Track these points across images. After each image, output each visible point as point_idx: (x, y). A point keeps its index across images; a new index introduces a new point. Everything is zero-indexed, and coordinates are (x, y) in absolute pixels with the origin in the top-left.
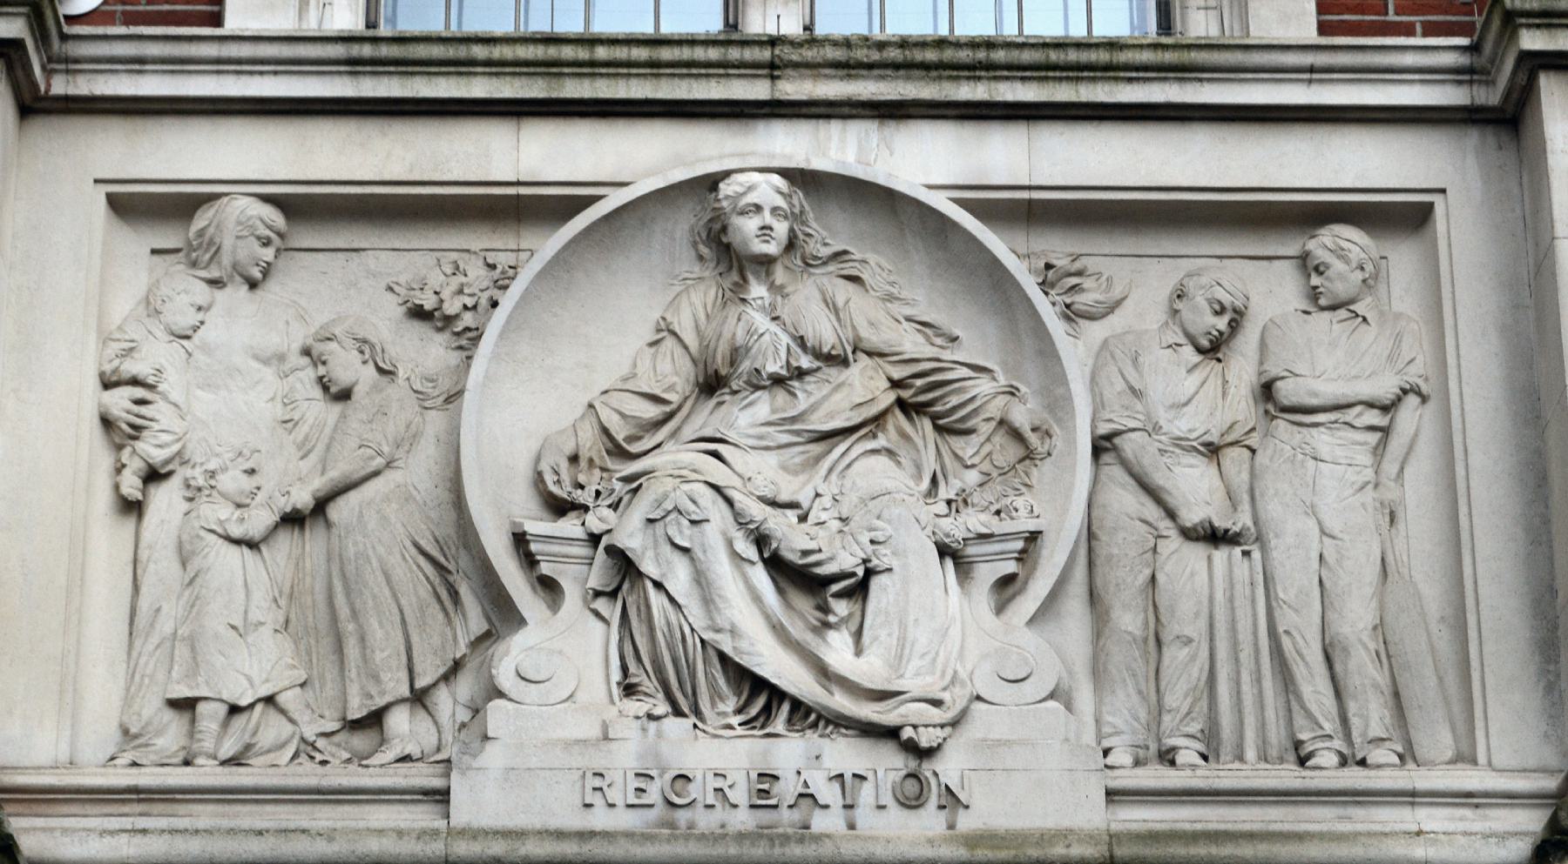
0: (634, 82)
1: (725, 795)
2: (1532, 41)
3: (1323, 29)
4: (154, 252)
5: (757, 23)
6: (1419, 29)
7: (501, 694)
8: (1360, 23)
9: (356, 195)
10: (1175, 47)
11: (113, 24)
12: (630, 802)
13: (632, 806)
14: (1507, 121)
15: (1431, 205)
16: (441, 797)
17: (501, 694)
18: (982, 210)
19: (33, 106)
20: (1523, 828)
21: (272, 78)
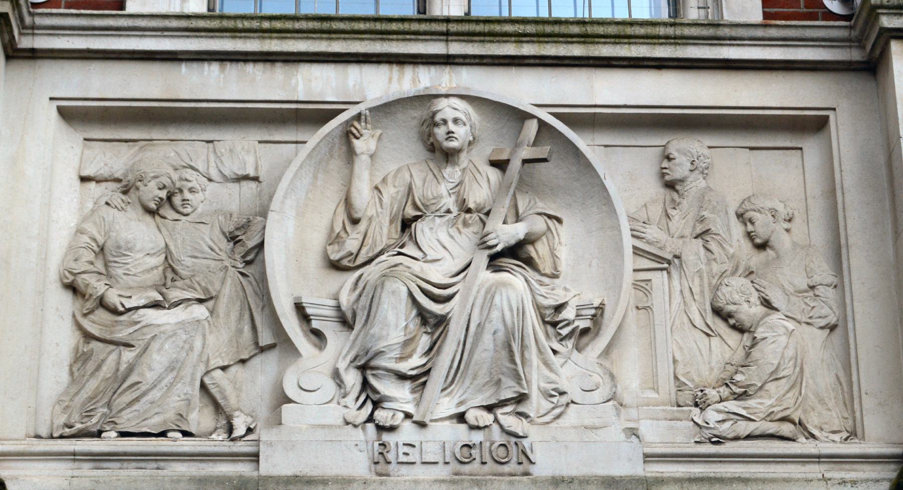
0: (657, 47)
1: (384, 457)
2: (888, 22)
3: (766, 16)
4: (85, 139)
5: (438, 10)
6: (820, 15)
7: (290, 401)
8: (776, 13)
9: (206, 108)
10: (426, 20)
11: (817, 20)
12: (400, 460)
13: (402, 463)
14: (872, 67)
15: (827, 117)
16: (255, 457)
17: (290, 401)
18: (571, 120)
19: (14, 54)
20: (886, 477)
21: (138, 39)
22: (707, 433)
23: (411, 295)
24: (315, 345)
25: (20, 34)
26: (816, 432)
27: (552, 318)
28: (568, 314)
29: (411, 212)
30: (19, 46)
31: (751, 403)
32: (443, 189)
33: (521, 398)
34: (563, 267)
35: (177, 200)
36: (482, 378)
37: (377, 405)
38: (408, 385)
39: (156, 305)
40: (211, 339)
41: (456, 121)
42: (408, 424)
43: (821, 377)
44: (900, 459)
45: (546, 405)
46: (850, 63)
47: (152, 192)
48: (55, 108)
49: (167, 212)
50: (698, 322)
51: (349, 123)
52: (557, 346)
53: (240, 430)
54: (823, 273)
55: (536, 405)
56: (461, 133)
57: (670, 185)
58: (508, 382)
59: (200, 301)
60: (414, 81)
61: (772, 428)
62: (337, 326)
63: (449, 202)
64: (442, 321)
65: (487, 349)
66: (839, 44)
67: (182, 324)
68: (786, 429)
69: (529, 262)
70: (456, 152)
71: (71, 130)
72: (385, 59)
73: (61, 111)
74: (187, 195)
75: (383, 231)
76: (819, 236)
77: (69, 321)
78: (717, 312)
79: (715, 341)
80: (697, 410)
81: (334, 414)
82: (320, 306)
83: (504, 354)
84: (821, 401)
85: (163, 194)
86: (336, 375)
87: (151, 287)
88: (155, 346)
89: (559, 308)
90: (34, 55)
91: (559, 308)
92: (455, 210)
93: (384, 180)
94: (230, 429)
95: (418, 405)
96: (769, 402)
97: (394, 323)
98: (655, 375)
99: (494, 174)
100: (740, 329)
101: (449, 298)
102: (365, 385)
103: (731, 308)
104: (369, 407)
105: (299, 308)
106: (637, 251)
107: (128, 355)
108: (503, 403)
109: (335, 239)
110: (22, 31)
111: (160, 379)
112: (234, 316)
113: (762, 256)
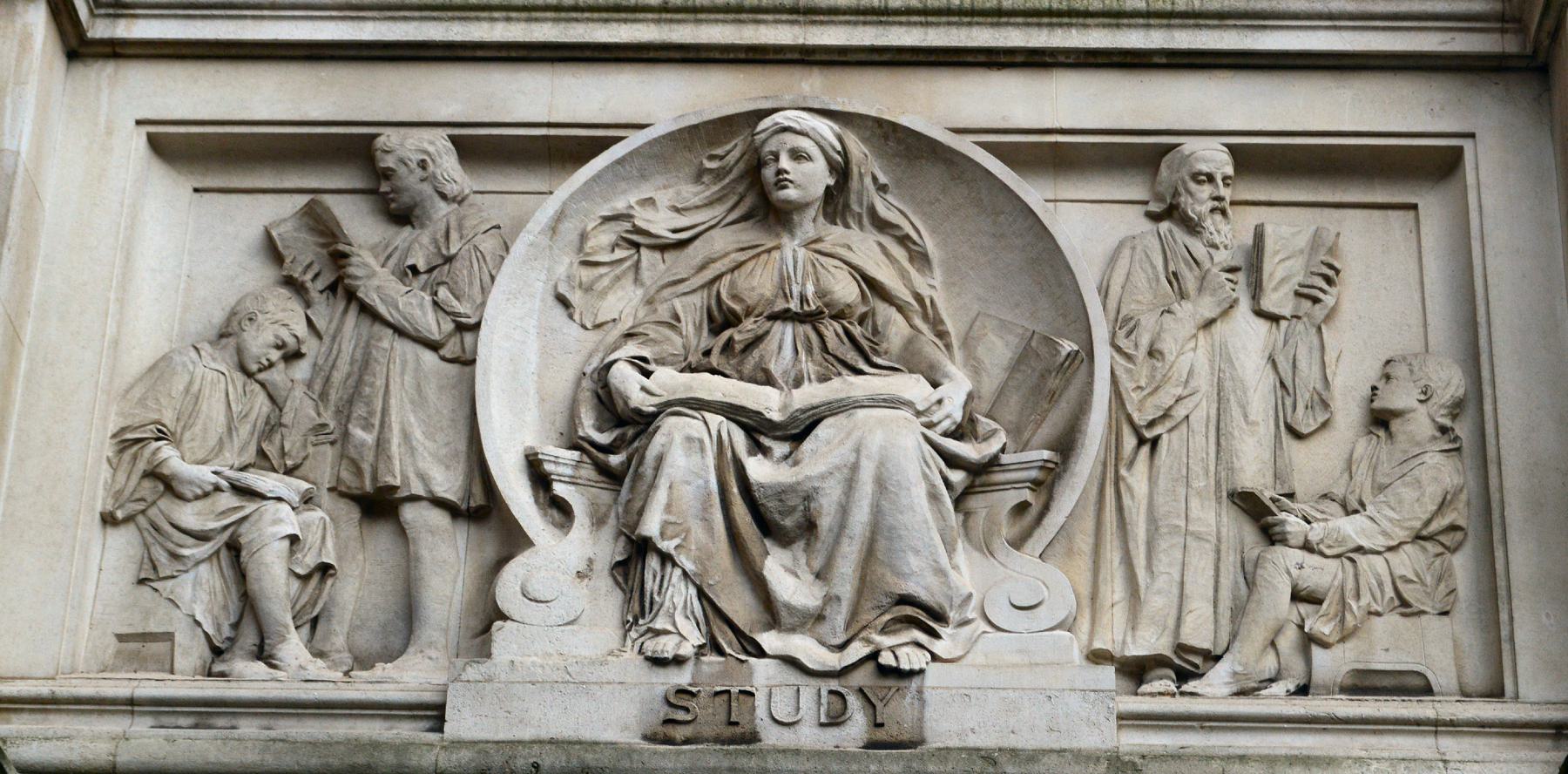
4: (196, 190)
7: (504, 617)
15: (1460, 150)
17: (504, 617)
24: (555, 524)
25: (92, 14)
30: (90, 35)
44: (1560, 731)
46: (1502, 57)
48: (144, 138)
66: (1478, 25)
71: (173, 174)
72: (108, 50)
87: (655, 416)
90: (117, 51)
110: (96, 12)
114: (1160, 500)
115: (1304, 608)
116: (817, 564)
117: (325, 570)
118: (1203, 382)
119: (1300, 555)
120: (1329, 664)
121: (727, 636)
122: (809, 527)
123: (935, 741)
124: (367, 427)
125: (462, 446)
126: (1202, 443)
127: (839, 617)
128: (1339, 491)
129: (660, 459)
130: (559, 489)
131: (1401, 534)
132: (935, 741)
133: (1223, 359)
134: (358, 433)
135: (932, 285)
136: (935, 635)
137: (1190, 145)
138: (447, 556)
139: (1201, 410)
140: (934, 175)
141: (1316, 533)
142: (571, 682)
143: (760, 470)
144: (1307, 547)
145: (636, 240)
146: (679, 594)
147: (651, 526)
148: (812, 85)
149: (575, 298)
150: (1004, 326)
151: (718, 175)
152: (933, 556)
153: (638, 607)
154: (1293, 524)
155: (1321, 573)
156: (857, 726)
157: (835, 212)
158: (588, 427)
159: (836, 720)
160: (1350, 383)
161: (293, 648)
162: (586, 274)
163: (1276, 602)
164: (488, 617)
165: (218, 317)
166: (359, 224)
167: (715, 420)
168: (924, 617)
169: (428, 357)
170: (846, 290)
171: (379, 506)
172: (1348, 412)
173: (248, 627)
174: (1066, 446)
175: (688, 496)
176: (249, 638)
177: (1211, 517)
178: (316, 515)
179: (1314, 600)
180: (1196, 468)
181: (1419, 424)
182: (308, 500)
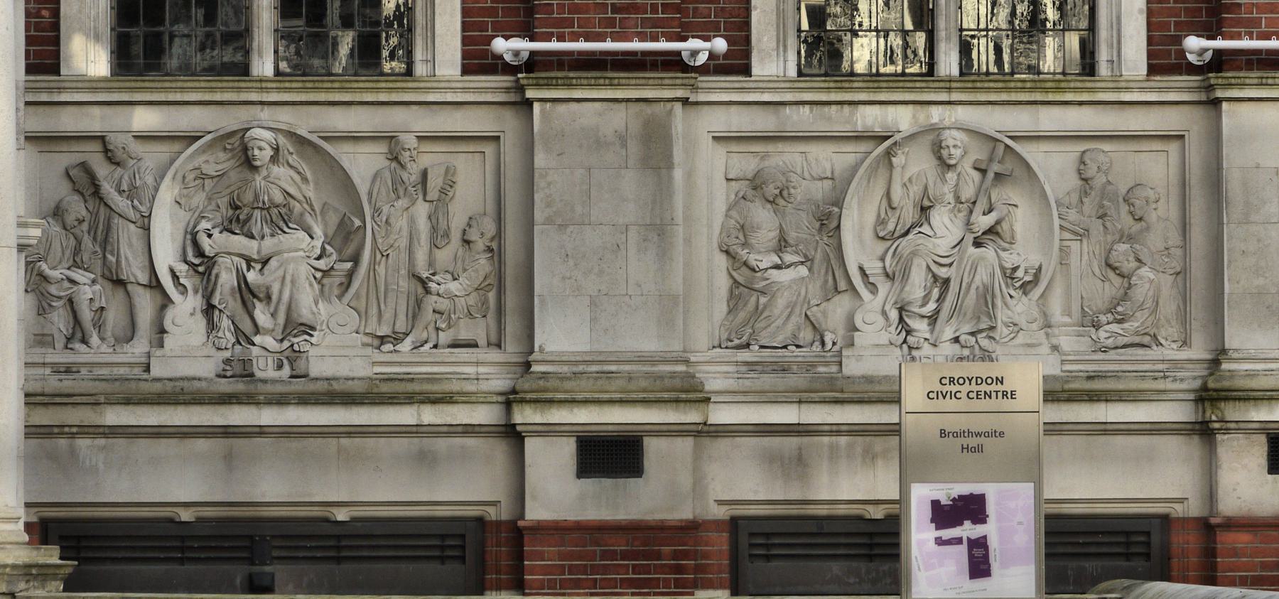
22: (1099, 345)
23: (928, 267)
26: (1163, 341)
27: (1010, 274)
28: (1020, 273)
29: (926, 203)
31: (1126, 325)
32: (946, 189)
33: (992, 328)
34: (1018, 237)
35: (785, 193)
36: (969, 315)
37: (909, 332)
38: (926, 320)
39: (777, 267)
40: (810, 287)
41: (955, 146)
42: (926, 344)
43: (1169, 307)
45: (1006, 331)
47: (771, 190)
49: (781, 202)
50: (1097, 271)
51: (890, 148)
52: (1013, 293)
53: (829, 346)
54: (1175, 238)
55: (1002, 331)
56: (957, 153)
57: (1085, 180)
58: (984, 319)
59: (802, 263)
60: (928, 117)
61: (1137, 339)
62: (882, 278)
63: (950, 197)
64: (947, 282)
65: (971, 300)
67: (794, 281)
68: (1146, 340)
69: (997, 234)
70: (955, 165)
73: (714, 138)
74: (792, 191)
75: (909, 215)
76: (1174, 213)
77: (725, 272)
78: (1109, 265)
79: (1107, 284)
80: (1093, 330)
81: (884, 338)
82: (873, 267)
83: (982, 301)
84: (1168, 321)
85: (777, 192)
86: (884, 313)
88: (779, 294)
89: (1015, 269)
91: (1015, 269)
92: (952, 201)
93: (910, 180)
94: (823, 344)
95: (932, 331)
96: (1136, 324)
97: (917, 284)
98: (1070, 307)
99: (976, 176)
100: (1122, 275)
101: (951, 265)
102: (901, 319)
103: (1117, 264)
104: (904, 334)
105: (861, 269)
106: (1061, 227)
107: (763, 300)
108: (980, 331)
109: (881, 222)
111: (782, 312)
112: (823, 271)
113: (1138, 226)
114: (389, 278)
115: (437, 316)
116: (272, 310)
117: (102, 308)
118: (405, 233)
119: (435, 298)
120: (444, 338)
121: (243, 338)
122: (269, 297)
123: (312, 375)
124: (113, 255)
125: (147, 264)
126: (404, 256)
127: (279, 329)
128: (451, 269)
129: (217, 276)
130: (182, 281)
131: (470, 289)
132: (312, 375)
133: (412, 221)
134: (109, 256)
135: (311, 194)
136: (311, 336)
137: (402, 137)
138: (145, 304)
139: (403, 243)
140: (310, 150)
141: (442, 289)
142: (186, 355)
143: (252, 276)
144: (438, 294)
145: (203, 177)
146: (226, 323)
147: (215, 302)
148: (265, 114)
149: (182, 202)
150: (336, 210)
151: (231, 150)
152: (308, 304)
153: (212, 326)
154: (433, 285)
155: (443, 304)
156: (286, 371)
157: (327, 52)
158: (191, 258)
159: (280, 367)
160: (457, 222)
161: (95, 340)
162: (185, 191)
163: (428, 315)
164: (161, 331)
165: (53, 205)
166: (102, 170)
167: (236, 259)
168: (308, 329)
169: (132, 226)
170: (278, 197)
171: (119, 283)
172: (456, 236)
173: (78, 334)
174: (356, 259)
175: (227, 288)
176: (79, 335)
177: (406, 285)
178: (98, 287)
179: (441, 313)
180: (402, 266)
181: (480, 245)
182: (94, 282)
